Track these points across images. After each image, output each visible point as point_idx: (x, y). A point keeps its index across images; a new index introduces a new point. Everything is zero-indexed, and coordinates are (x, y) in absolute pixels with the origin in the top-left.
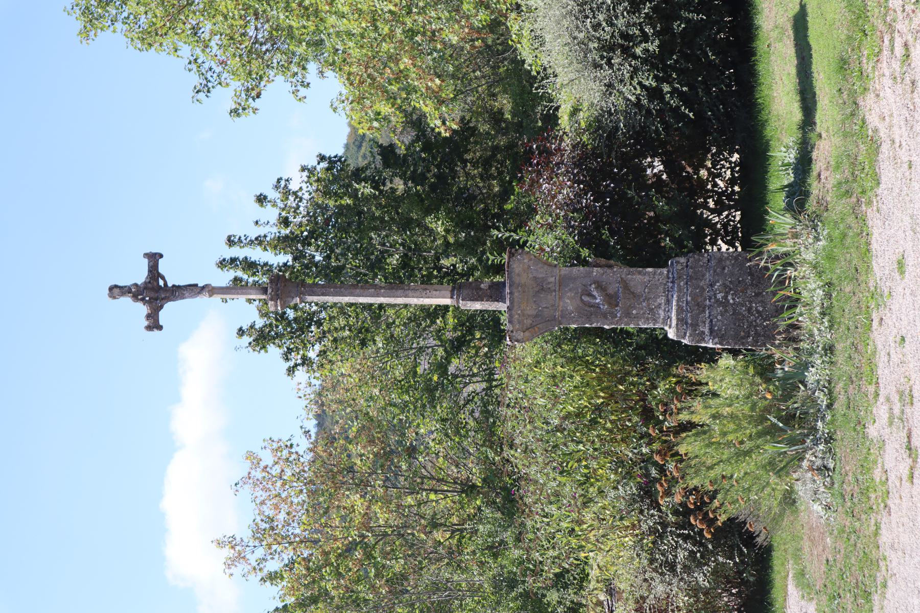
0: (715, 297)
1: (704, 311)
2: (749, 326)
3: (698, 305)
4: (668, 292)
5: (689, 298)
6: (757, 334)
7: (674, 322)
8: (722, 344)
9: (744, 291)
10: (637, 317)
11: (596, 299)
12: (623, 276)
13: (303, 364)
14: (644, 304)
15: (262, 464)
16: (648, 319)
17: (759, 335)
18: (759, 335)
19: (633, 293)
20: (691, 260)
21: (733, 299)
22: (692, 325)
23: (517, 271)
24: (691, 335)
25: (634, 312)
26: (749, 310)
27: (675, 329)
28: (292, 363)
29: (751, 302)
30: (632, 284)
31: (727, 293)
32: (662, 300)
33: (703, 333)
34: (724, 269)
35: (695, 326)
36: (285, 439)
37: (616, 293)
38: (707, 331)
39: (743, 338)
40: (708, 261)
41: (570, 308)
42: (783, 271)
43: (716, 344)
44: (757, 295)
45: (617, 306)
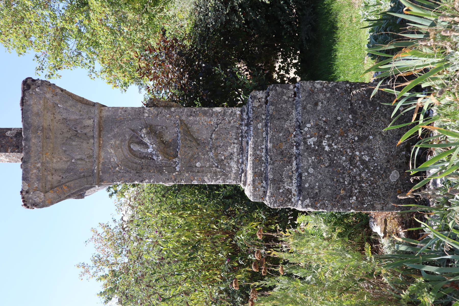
0: (305, 143)
1: (290, 162)
2: (352, 182)
3: (282, 153)
4: (242, 137)
5: (270, 145)
6: (362, 192)
7: (250, 178)
8: (315, 208)
9: (344, 134)
10: (202, 171)
11: (148, 147)
12: (183, 118)
13: (115, 193)
14: (211, 154)
15: (98, 233)
16: (216, 173)
17: (365, 194)
18: (365, 194)
19: (196, 140)
20: (271, 93)
21: (330, 145)
22: (273, 181)
23: (35, 109)
24: (272, 195)
25: (198, 164)
26: (351, 160)
27: (251, 187)
28: (111, 193)
29: (353, 149)
30: (195, 128)
31: (321, 137)
32: (234, 149)
33: (289, 191)
34: (316, 104)
35: (277, 182)
36: (105, 223)
37: (175, 140)
38: (294, 189)
39: (343, 198)
40: (295, 94)
41: (114, 159)
42: (409, 100)
43: (307, 206)
44: (362, 139)
45: (176, 156)
